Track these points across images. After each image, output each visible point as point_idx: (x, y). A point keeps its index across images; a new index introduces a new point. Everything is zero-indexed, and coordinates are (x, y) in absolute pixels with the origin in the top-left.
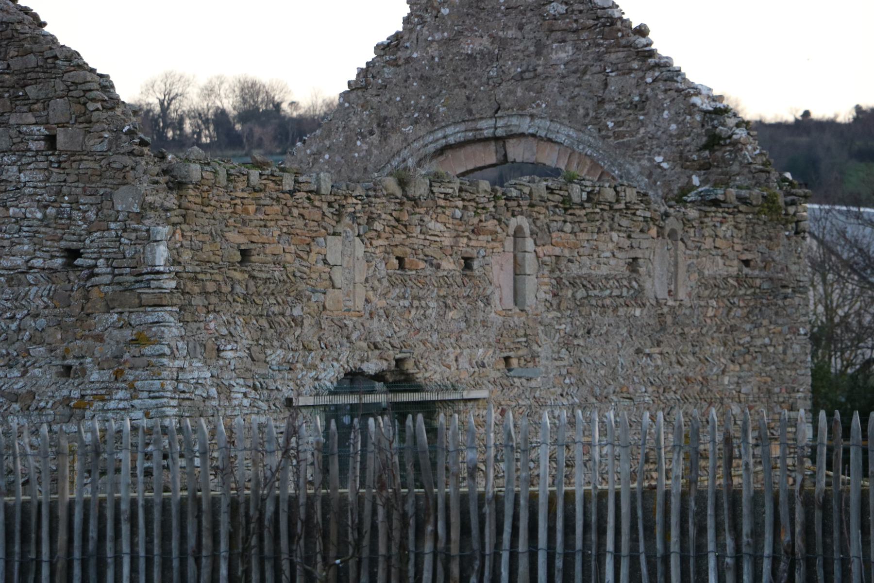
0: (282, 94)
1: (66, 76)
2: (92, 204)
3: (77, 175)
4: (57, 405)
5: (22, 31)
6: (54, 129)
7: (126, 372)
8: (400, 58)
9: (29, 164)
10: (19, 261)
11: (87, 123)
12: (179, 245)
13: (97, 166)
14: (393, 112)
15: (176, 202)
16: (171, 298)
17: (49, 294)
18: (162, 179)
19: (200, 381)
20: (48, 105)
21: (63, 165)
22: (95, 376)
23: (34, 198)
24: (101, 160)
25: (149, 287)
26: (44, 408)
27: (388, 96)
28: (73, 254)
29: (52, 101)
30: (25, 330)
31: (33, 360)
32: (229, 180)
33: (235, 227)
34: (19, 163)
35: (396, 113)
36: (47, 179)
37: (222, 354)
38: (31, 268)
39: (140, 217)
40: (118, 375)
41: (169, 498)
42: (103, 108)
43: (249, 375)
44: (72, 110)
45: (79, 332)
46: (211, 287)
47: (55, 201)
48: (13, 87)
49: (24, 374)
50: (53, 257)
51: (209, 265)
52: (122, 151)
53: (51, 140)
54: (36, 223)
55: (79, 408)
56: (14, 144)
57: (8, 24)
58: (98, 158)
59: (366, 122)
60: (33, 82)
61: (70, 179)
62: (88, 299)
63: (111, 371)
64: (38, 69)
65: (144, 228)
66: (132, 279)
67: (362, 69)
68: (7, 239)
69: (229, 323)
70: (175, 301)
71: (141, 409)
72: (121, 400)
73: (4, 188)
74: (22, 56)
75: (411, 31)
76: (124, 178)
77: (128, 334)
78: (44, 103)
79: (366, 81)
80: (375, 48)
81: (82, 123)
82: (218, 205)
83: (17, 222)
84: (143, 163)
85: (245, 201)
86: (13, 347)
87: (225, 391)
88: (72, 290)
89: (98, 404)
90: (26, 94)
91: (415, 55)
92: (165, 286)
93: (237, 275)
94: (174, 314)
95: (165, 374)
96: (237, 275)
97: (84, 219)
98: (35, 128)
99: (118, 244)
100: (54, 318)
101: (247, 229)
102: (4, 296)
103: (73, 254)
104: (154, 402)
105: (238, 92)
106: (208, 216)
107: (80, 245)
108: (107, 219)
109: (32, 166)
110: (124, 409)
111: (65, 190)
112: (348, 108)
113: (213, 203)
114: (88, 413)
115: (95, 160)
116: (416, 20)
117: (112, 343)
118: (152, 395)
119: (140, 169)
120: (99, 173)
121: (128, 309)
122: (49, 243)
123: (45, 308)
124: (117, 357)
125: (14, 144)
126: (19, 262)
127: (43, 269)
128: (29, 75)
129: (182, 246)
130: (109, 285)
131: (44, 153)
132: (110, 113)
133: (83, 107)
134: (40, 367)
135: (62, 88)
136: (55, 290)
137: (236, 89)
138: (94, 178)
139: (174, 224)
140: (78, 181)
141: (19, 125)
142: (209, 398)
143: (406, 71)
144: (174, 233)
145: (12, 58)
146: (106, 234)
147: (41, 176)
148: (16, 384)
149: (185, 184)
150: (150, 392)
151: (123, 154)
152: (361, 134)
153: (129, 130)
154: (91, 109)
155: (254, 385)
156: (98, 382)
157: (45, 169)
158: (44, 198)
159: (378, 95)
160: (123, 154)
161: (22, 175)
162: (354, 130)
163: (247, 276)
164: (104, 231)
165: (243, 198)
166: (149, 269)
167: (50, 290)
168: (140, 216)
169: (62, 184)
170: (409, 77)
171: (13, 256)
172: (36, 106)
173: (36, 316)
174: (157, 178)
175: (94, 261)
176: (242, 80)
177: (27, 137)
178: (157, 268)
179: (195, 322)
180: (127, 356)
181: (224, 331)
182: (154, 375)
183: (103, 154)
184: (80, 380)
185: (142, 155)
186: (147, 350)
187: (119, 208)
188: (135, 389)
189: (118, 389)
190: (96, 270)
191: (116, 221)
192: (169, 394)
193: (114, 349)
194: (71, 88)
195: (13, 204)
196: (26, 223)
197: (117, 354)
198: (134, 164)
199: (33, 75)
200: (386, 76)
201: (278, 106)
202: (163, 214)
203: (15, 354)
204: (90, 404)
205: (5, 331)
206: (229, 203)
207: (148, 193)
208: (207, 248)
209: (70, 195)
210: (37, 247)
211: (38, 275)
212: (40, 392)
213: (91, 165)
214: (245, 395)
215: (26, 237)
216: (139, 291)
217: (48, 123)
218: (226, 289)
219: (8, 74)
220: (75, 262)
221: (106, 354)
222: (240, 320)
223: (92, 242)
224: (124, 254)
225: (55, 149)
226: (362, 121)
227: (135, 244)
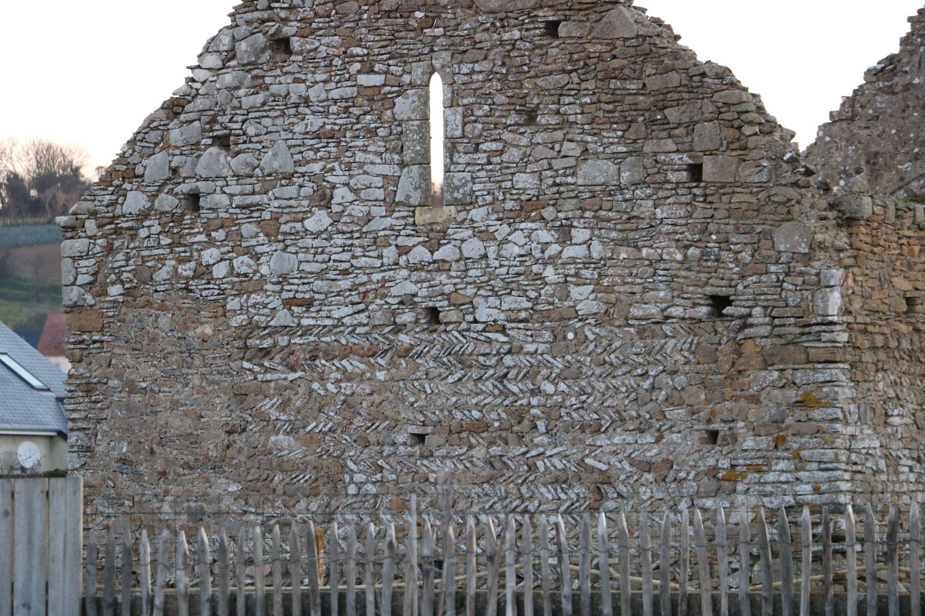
0: (81, 158)
1: (716, 96)
2: (745, 244)
3: (727, 210)
4: (702, 476)
5: (662, 45)
6: (701, 157)
7: (789, 439)
8: (897, 84)
9: (668, 197)
10: (653, 310)
11: (741, 150)
12: (851, 291)
13: (753, 200)
14: (886, 146)
15: (848, 241)
16: (844, 354)
17: (690, 347)
18: (832, 214)
19: (870, 452)
20: (693, 130)
21: (709, 199)
22: (749, 443)
23: (672, 237)
24: (758, 192)
25: (819, 340)
26: (685, 479)
27: (881, 128)
28: (719, 303)
29: (699, 125)
30: (661, 389)
31: (670, 423)
32: (897, 217)
33: (902, 271)
34: (655, 197)
35: (890, 148)
36: (690, 216)
37: (890, 420)
38: (667, 318)
39: (808, 258)
40: (779, 442)
41: (363, 592)
42: (761, 132)
43: (914, 445)
44: (723, 135)
45: (728, 391)
46: (879, 341)
47: (700, 240)
48: (649, 110)
49: (658, 440)
50: (695, 305)
51: (877, 315)
52: (784, 182)
53: (696, 171)
54: (675, 265)
55: (729, 480)
56: (649, 175)
57: (644, 37)
58: (755, 190)
59: (852, 158)
60: (674, 103)
61: (718, 215)
62: (740, 354)
63: (770, 438)
64: (682, 89)
65: (814, 271)
66: (798, 330)
67: (848, 98)
68: (638, 284)
69: (896, 384)
70: (848, 357)
71: (808, 483)
72: (783, 471)
73: (635, 225)
74: (661, 74)
75: (912, 53)
76: (789, 213)
77: (792, 395)
78: (687, 127)
79: (853, 111)
80: (865, 73)
81: (736, 150)
82: (887, 244)
83: (650, 265)
84: (810, 195)
85: (912, 241)
86: (645, 408)
87: (893, 462)
88: (719, 344)
89: (753, 476)
90: (666, 117)
91: (916, 81)
92: (839, 339)
93: (903, 328)
94: (846, 372)
95: (839, 442)
96: (903, 328)
97: (736, 261)
98: (676, 157)
99: (779, 290)
100: (697, 376)
101: (911, 274)
102: (634, 350)
103: (719, 303)
104: (826, 474)
105: (32, 155)
106: (877, 258)
107: (731, 291)
108: (766, 261)
109: (671, 200)
110: (787, 482)
111: (712, 227)
112: (829, 142)
113: (882, 242)
114: (740, 487)
115: (751, 193)
116: (919, 40)
117: (771, 405)
118: (823, 466)
119: (807, 203)
120: (756, 207)
121: (792, 366)
122: (691, 289)
123: (686, 363)
124: (777, 422)
125: (649, 175)
126: (654, 311)
127: (684, 319)
128: (669, 95)
129: (853, 293)
130: (767, 337)
131: (686, 185)
132: (767, 138)
133: (737, 132)
134: (679, 432)
135: (711, 110)
136: (698, 343)
137: (30, 152)
138: (750, 213)
139: (846, 267)
140: (729, 217)
141: (655, 154)
142: (876, 472)
143: (905, 99)
144: (847, 277)
145: (648, 76)
146: (764, 278)
147: (682, 212)
148: (649, 451)
149: (857, 220)
150: (820, 462)
151: (785, 185)
152: (845, 172)
153: (791, 157)
154: (748, 133)
155: (919, 457)
156: (753, 450)
157: (687, 204)
158: (686, 237)
159: (868, 128)
160: (785, 185)
161: (658, 210)
162: (837, 167)
163: (911, 328)
164: (761, 275)
165: (909, 237)
166: (819, 319)
167: (691, 344)
168: (808, 257)
169: (709, 220)
170: (908, 106)
171: (646, 303)
172: (677, 132)
173: (674, 373)
174: (825, 213)
175: (748, 310)
176: (37, 143)
177: (665, 167)
178: (830, 318)
179: (865, 381)
180: (789, 420)
181: (891, 393)
182: (826, 443)
183: (762, 186)
184: (731, 447)
185: (807, 186)
186: (817, 414)
187: (782, 248)
188: (801, 458)
189: (779, 458)
190: (750, 320)
191: (777, 263)
192: (843, 466)
193: (773, 412)
194: (722, 110)
195: (647, 243)
196: (662, 266)
197: (777, 417)
198: (799, 197)
199: (675, 96)
200: (878, 105)
201: (76, 171)
202: (834, 255)
203: (648, 416)
204: (743, 476)
205: (635, 390)
206: (897, 242)
207: (817, 230)
208: (876, 295)
209: (718, 233)
210: (676, 293)
211: (677, 326)
212: (680, 460)
213: (746, 198)
214: (911, 469)
215: (661, 282)
216: (805, 344)
217: (692, 151)
218: (893, 344)
219: (643, 94)
220: (724, 311)
221: (763, 418)
222: (906, 380)
223: (745, 287)
224: (785, 301)
225: (701, 181)
226: (846, 157)
227: (801, 290)
